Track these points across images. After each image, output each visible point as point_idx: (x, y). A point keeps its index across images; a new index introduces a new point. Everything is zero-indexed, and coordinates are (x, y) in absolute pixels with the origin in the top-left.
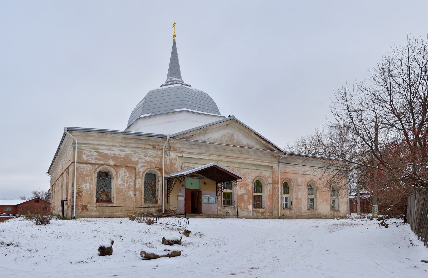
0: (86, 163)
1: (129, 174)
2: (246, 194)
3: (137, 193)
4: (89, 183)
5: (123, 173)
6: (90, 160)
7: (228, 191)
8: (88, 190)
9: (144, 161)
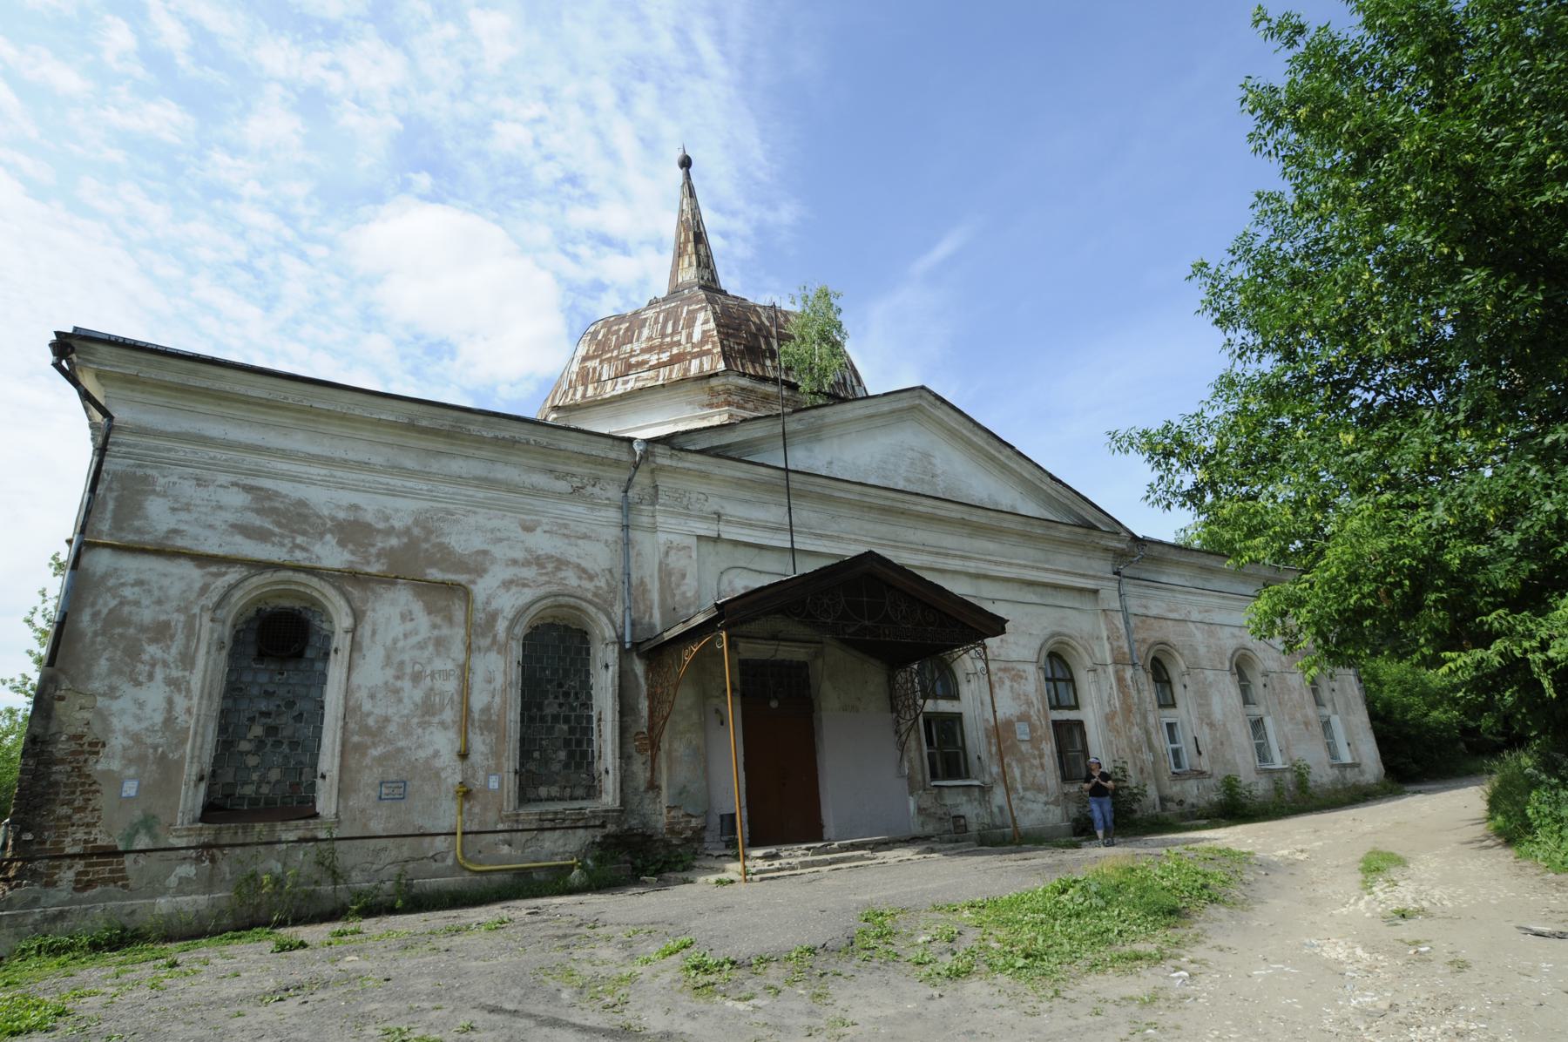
0: (161, 552)
1: (435, 626)
2: (1020, 719)
3: (479, 744)
4: (170, 682)
5: (395, 617)
6: (192, 530)
7: (945, 706)
8: (151, 730)
9: (519, 555)
